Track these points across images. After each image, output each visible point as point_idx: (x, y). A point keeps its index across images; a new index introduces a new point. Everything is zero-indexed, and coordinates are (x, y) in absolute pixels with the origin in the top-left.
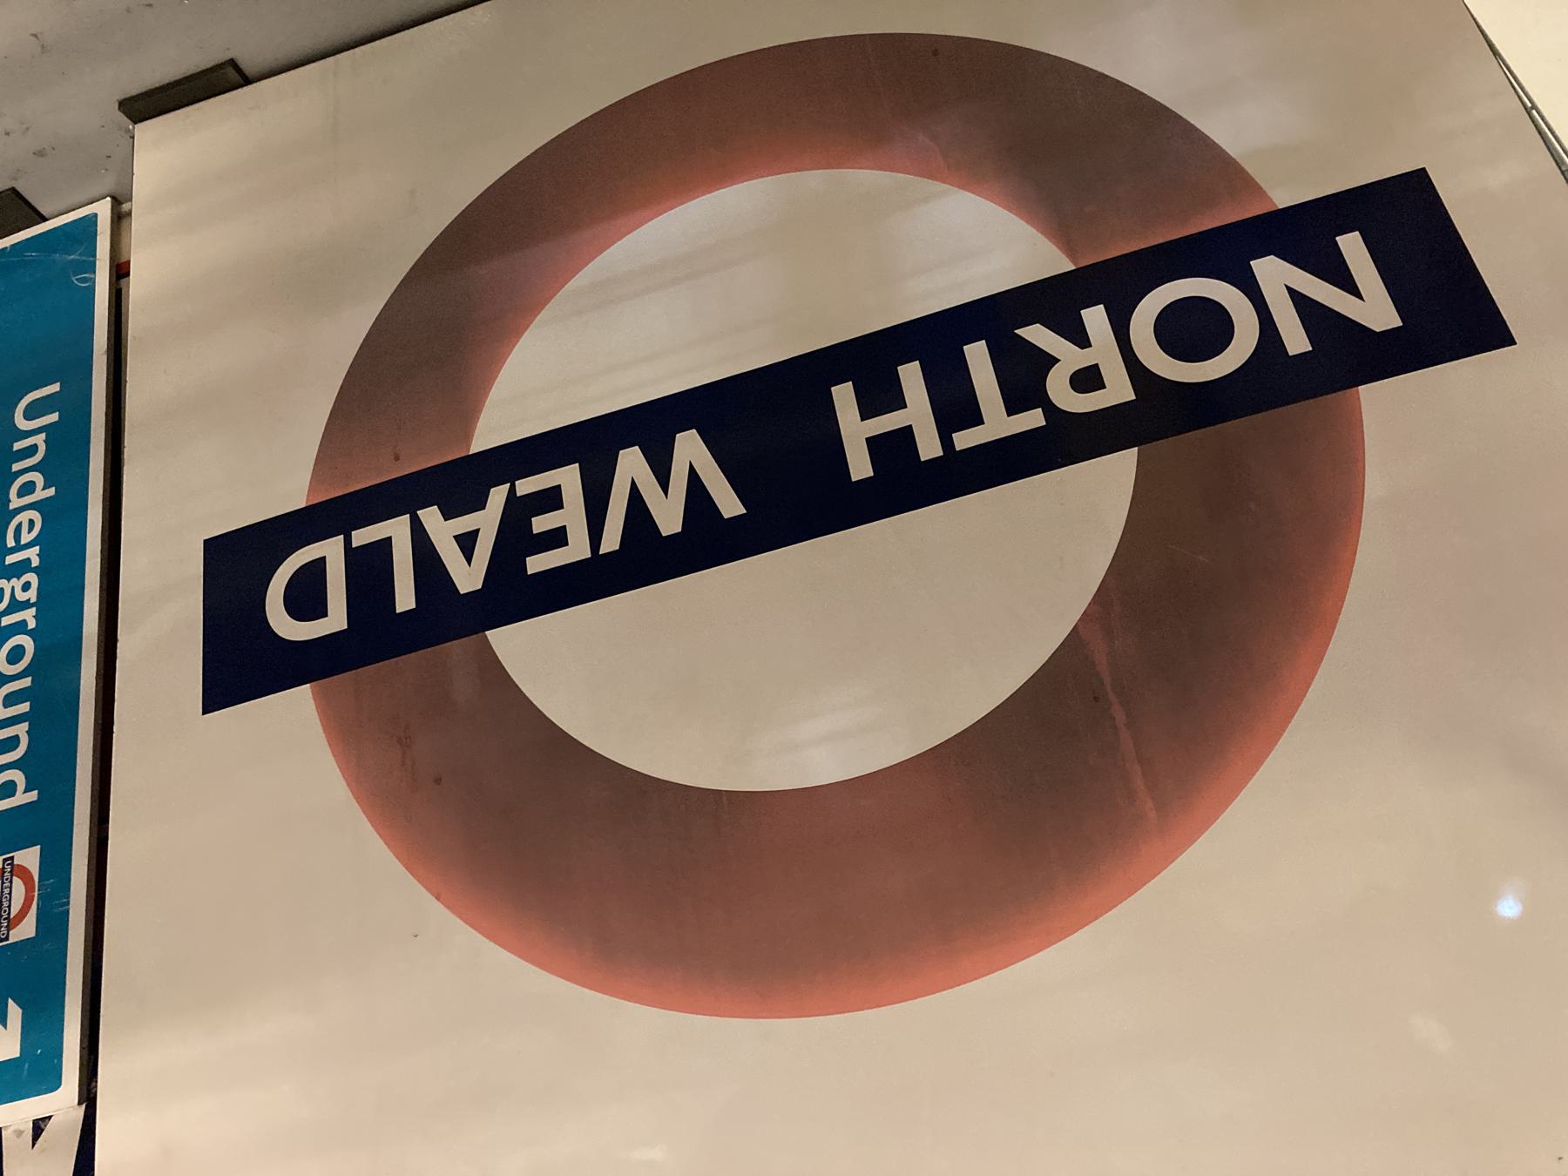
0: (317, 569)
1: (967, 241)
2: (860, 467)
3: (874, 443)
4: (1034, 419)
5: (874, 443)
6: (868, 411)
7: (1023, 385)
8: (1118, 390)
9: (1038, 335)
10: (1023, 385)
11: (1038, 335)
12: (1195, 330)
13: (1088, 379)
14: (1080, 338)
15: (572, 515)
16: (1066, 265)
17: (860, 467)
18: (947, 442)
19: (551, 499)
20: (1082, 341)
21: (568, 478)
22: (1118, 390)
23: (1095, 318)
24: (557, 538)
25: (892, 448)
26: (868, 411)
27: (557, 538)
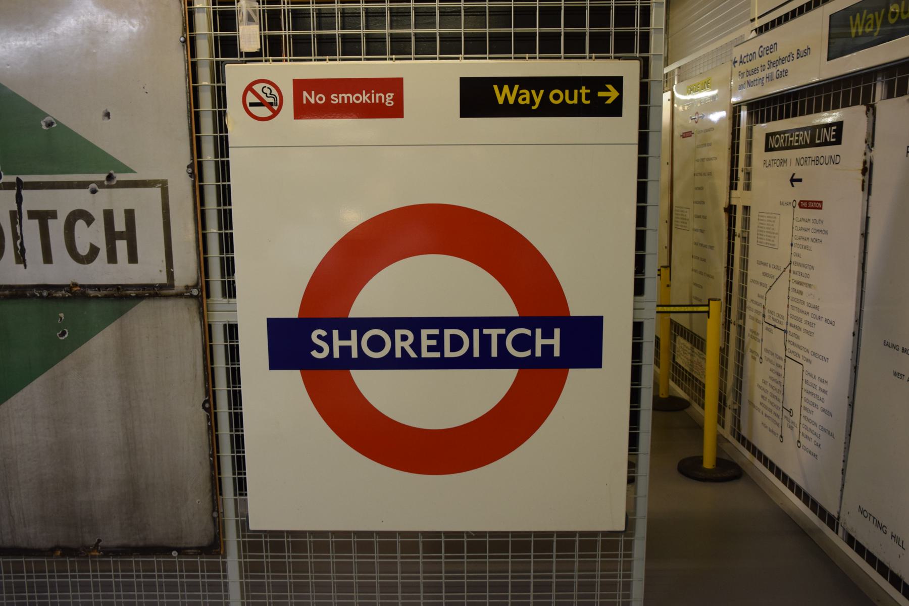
0: (453, 349)
1: (379, 389)
2: (557, 332)
3: (552, 337)
4: (486, 331)
5: (552, 337)
6: (551, 347)
7: (485, 341)
8: (398, 333)
9: (413, 355)
10: (485, 341)
11: (413, 355)
12: (376, 344)
13: (404, 338)
14: (403, 350)
15: (425, 343)
16: (353, 372)
17: (557, 332)
18: (534, 333)
19: (430, 349)
20: (403, 349)
21: (425, 354)
22: (398, 333)
23: (398, 354)
24: (430, 337)
25: (548, 334)
26: (551, 347)
27: (430, 337)
